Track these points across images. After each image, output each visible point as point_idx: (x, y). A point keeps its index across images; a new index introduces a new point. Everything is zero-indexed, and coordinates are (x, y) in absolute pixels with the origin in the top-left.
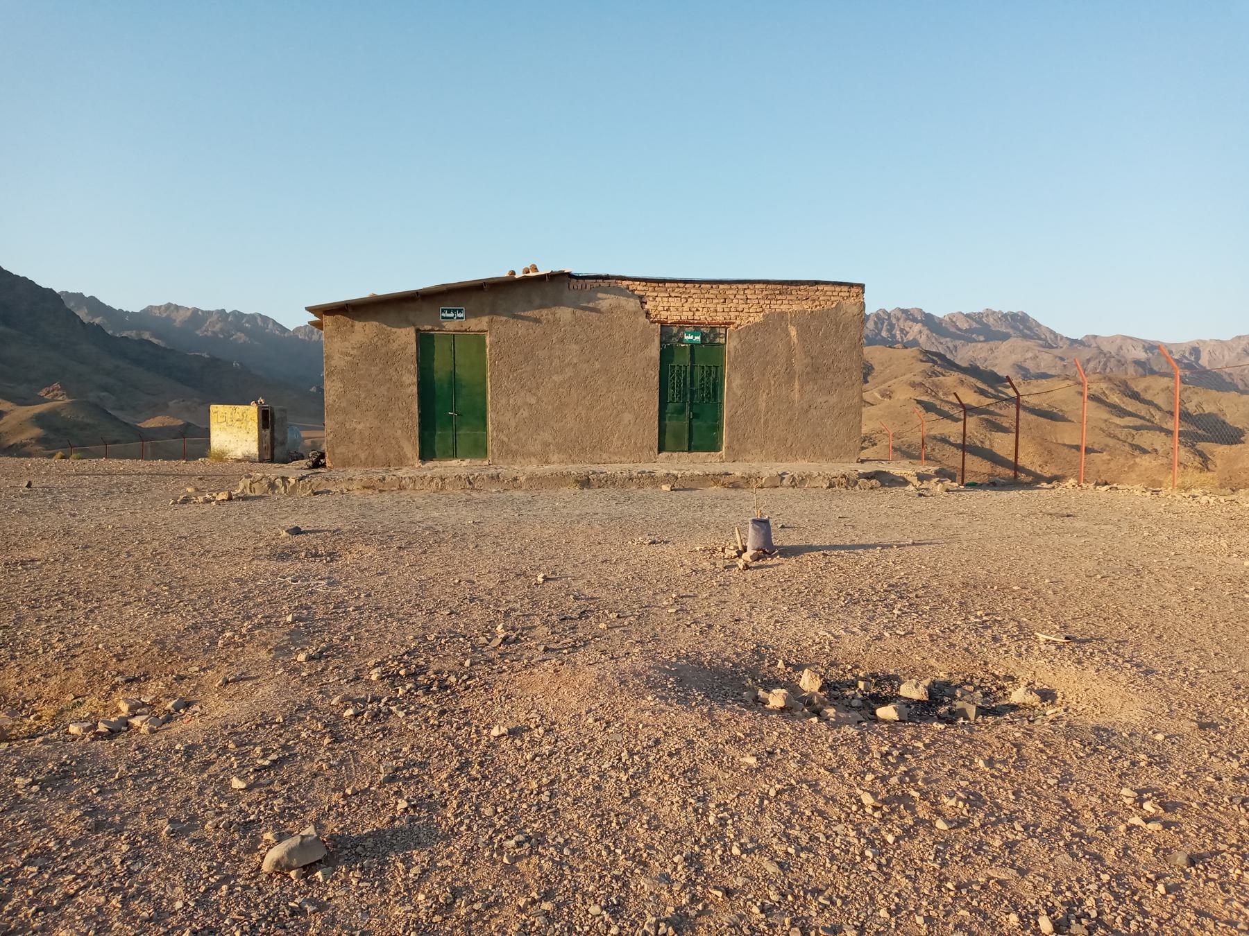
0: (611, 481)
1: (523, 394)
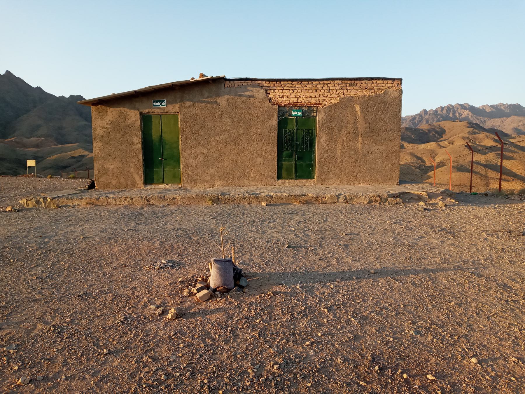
1: (199, 147)
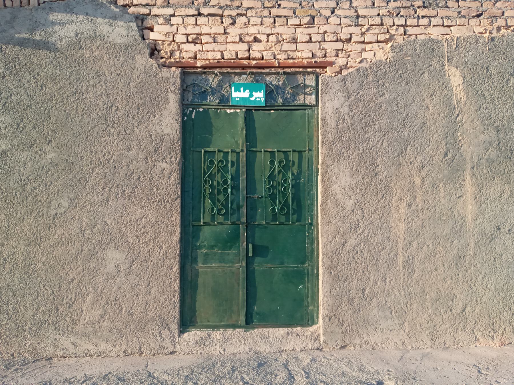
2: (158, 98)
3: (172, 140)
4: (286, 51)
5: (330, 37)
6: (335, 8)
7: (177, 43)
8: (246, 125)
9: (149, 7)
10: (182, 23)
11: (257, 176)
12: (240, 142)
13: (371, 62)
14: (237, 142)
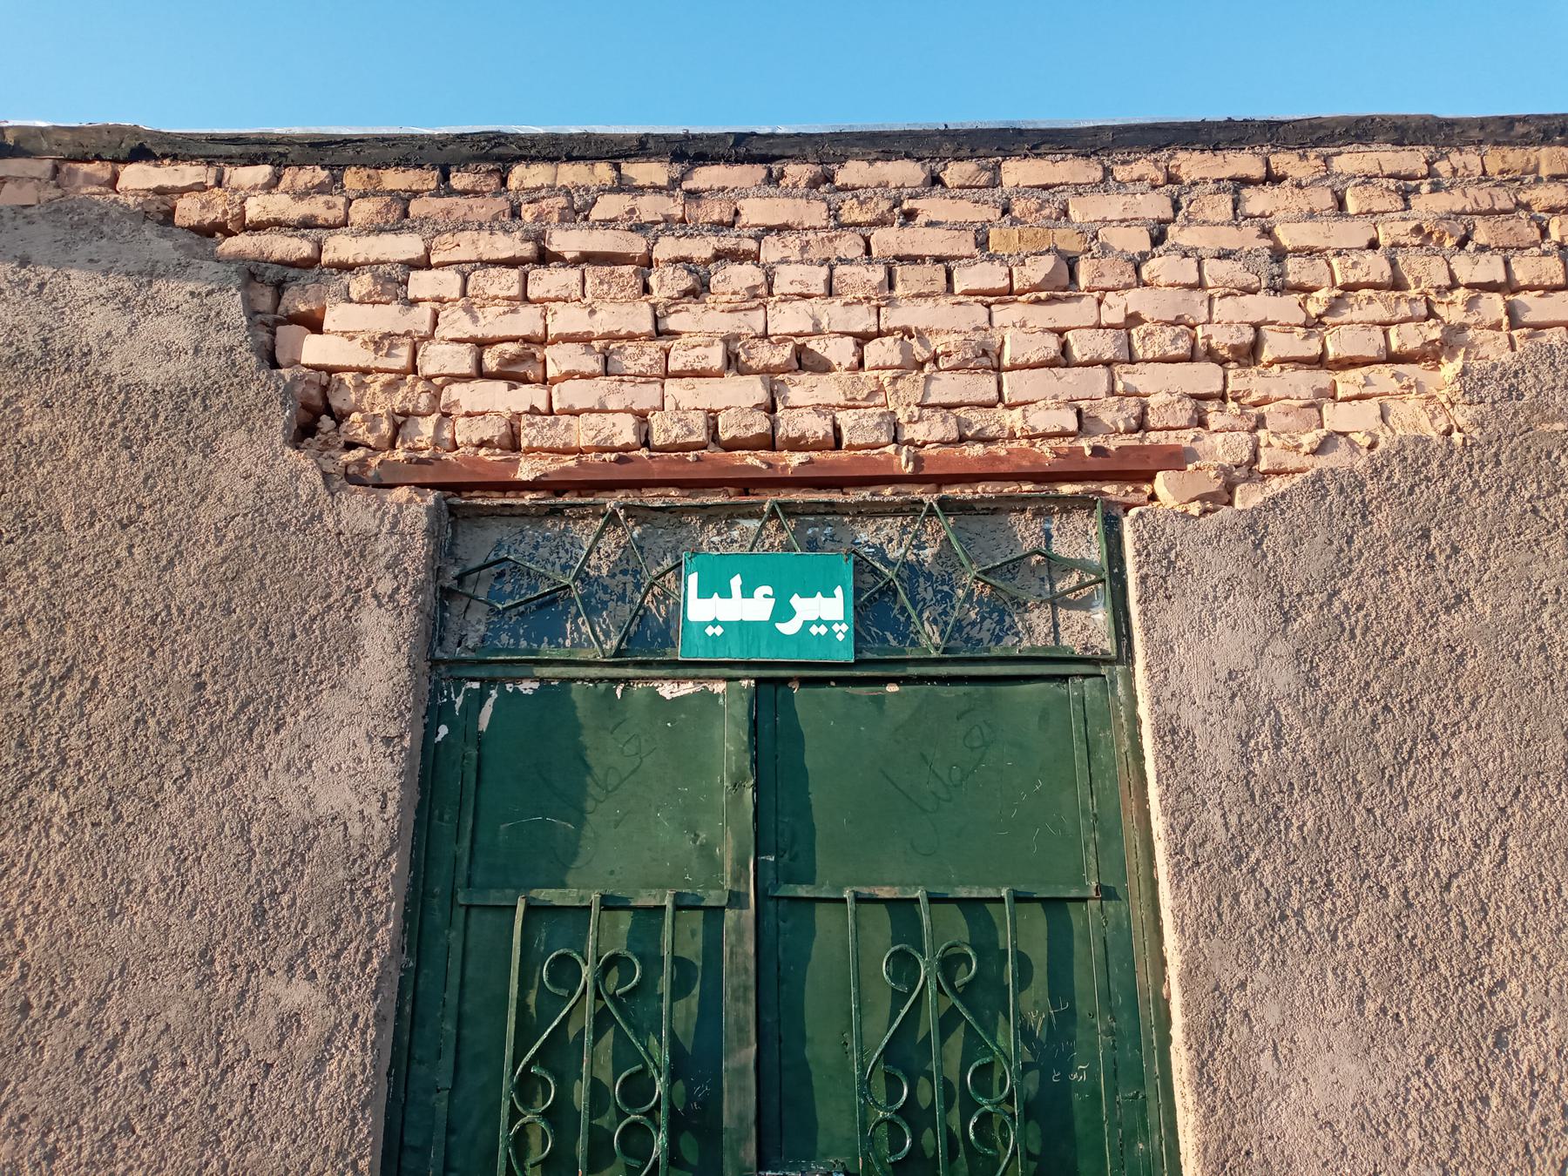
0: (514, 340)
2: (307, 630)
3: (356, 851)
4: (949, 407)
5: (1157, 339)
6: (1168, 222)
7: (429, 379)
8: (755, 761)
9: (313, 234)
10: (456, 294)
11: (820, 1048)
12: (727, 852)
13: (1371, 447)
14: (706, 851)
